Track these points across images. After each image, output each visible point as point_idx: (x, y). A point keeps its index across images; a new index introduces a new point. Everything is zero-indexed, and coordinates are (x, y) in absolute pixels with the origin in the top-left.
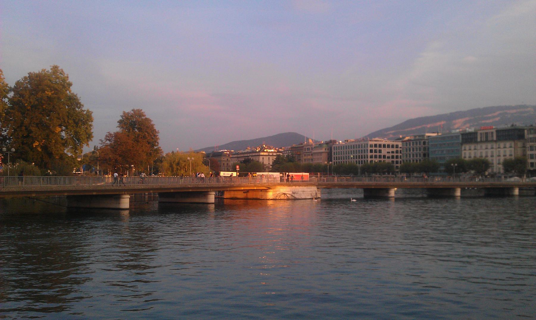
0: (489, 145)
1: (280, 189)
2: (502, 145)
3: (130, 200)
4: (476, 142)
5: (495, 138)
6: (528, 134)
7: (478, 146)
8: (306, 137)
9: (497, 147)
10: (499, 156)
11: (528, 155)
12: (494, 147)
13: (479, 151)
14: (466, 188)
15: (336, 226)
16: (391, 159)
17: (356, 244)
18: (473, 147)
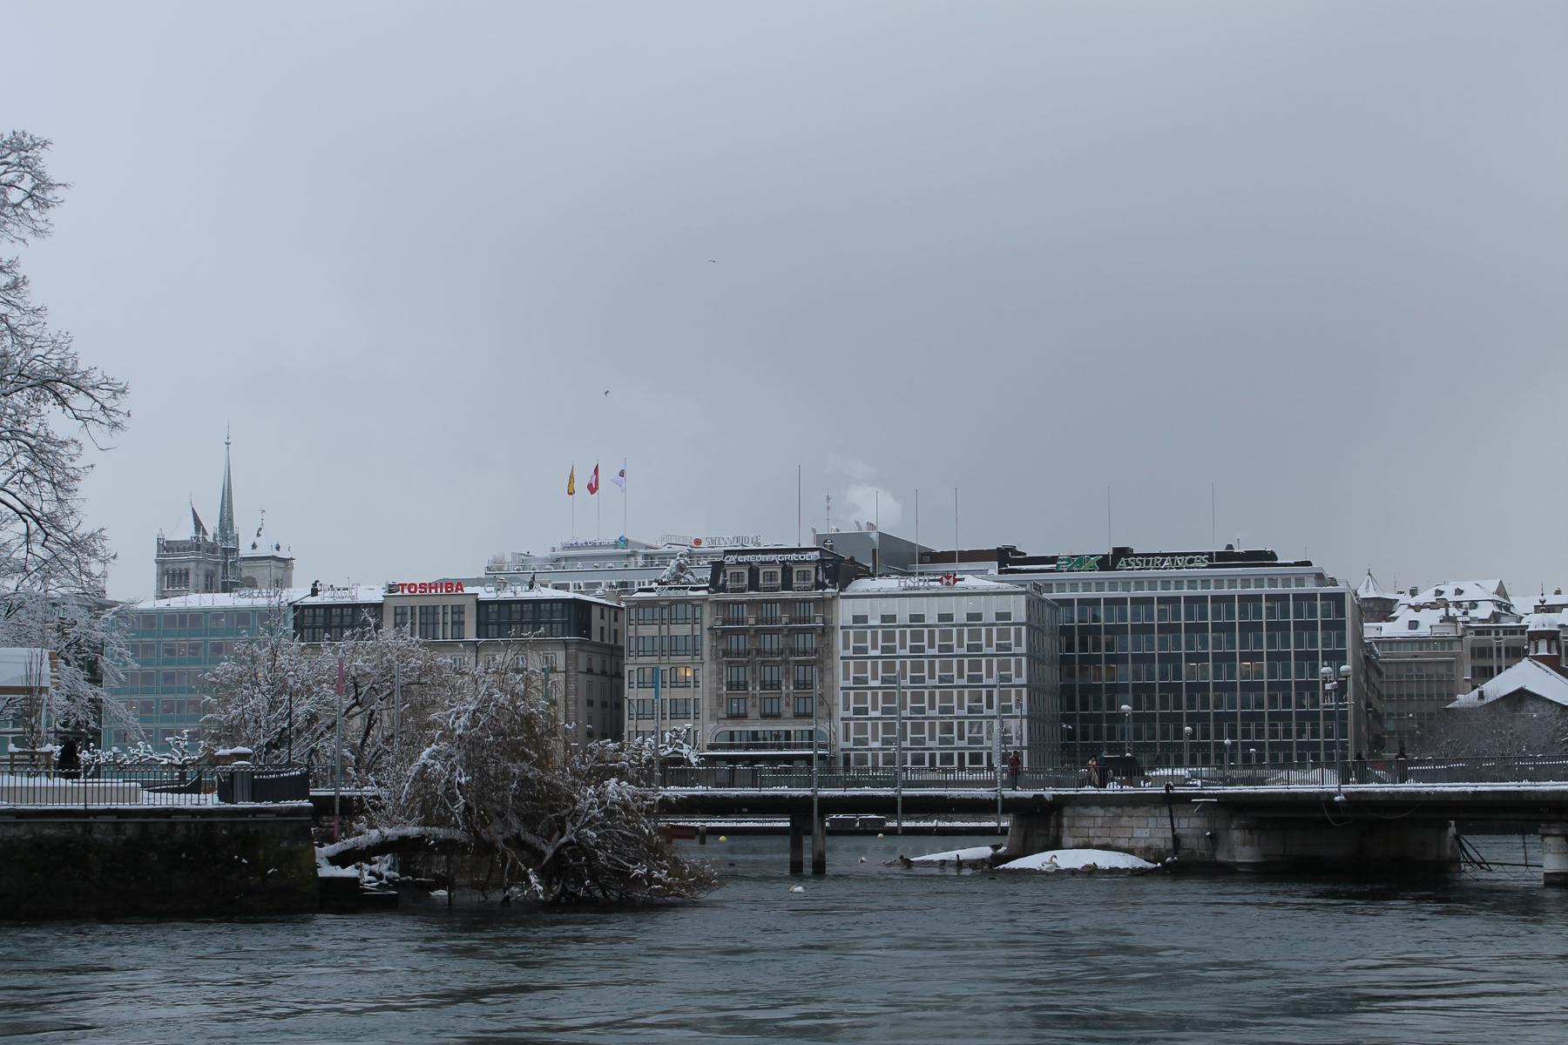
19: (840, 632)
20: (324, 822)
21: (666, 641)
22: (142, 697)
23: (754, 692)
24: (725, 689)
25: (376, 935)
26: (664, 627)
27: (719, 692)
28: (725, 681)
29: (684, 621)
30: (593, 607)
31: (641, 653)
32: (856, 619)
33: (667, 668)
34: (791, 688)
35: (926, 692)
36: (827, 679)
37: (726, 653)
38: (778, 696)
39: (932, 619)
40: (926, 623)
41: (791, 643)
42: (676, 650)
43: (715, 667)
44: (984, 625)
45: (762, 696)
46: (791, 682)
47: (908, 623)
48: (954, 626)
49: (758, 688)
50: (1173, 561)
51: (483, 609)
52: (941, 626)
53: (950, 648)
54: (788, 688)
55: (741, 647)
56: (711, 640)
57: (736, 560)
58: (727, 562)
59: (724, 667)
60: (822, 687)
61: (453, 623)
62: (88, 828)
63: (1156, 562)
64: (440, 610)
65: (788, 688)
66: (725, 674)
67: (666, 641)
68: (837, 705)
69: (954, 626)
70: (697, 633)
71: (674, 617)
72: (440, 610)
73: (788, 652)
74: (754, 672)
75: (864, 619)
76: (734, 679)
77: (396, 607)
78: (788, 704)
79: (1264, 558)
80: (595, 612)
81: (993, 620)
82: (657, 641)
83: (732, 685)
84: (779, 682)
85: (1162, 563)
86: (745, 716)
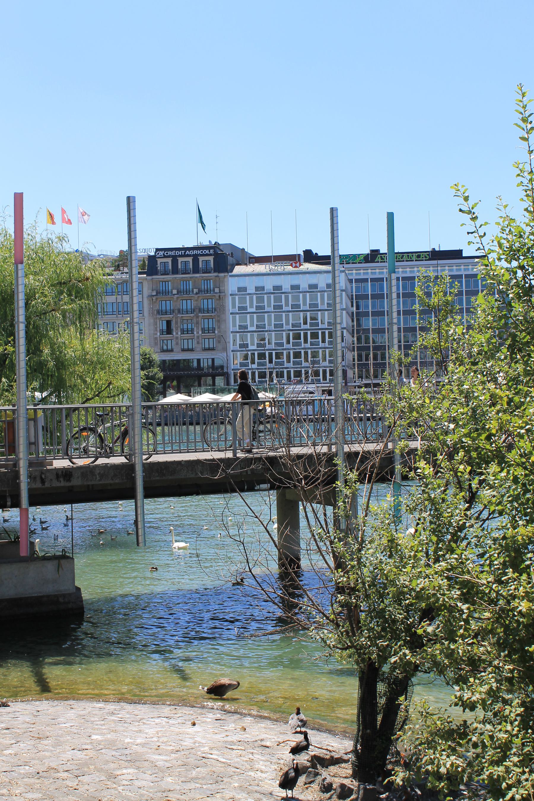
19: (230, 298)
20: (493, 677)
21: (120, 304)
22: (275, 454)
23: (177, 336)
24: (158, 334)
25: (302, 761)
27: (155, 336)
28: (158, 329)
29: (111, 294)
31: (106, 313)
32: (240, 289)
34: (200, 332)
35: (320, 332)
36: (223, 327)
38: (213, 337)
39: (251, 290)
40: (283, 291)
41: (199, 305)
42: (127, 311)
43: (152, 321)
44: (319, 292)
45: (203, 337)
46: (200, 328)
47: (272, 291)
48: (300, 292)
49: (179, 333)
50: (408, 256)
52: (293, 293)
54: (198, 333)
56: (150, 304)
57: (164, 254)
58: (158, 256)
59: (158, 320)
63: (398, 257)
65: (198, 333)
66: (158, 326)
67: (120, 304)
68: (229, 342)
69: (300, 292)
71: (125, 290)
73: (176, 311)
75: (245, 289)
76: (206, 326)
78: (198, 343)
79: (457, 254)
81: (254, 291)
82: (115, 305)
83: (183, 331)
84: (192, 330)
85: (402, 258)
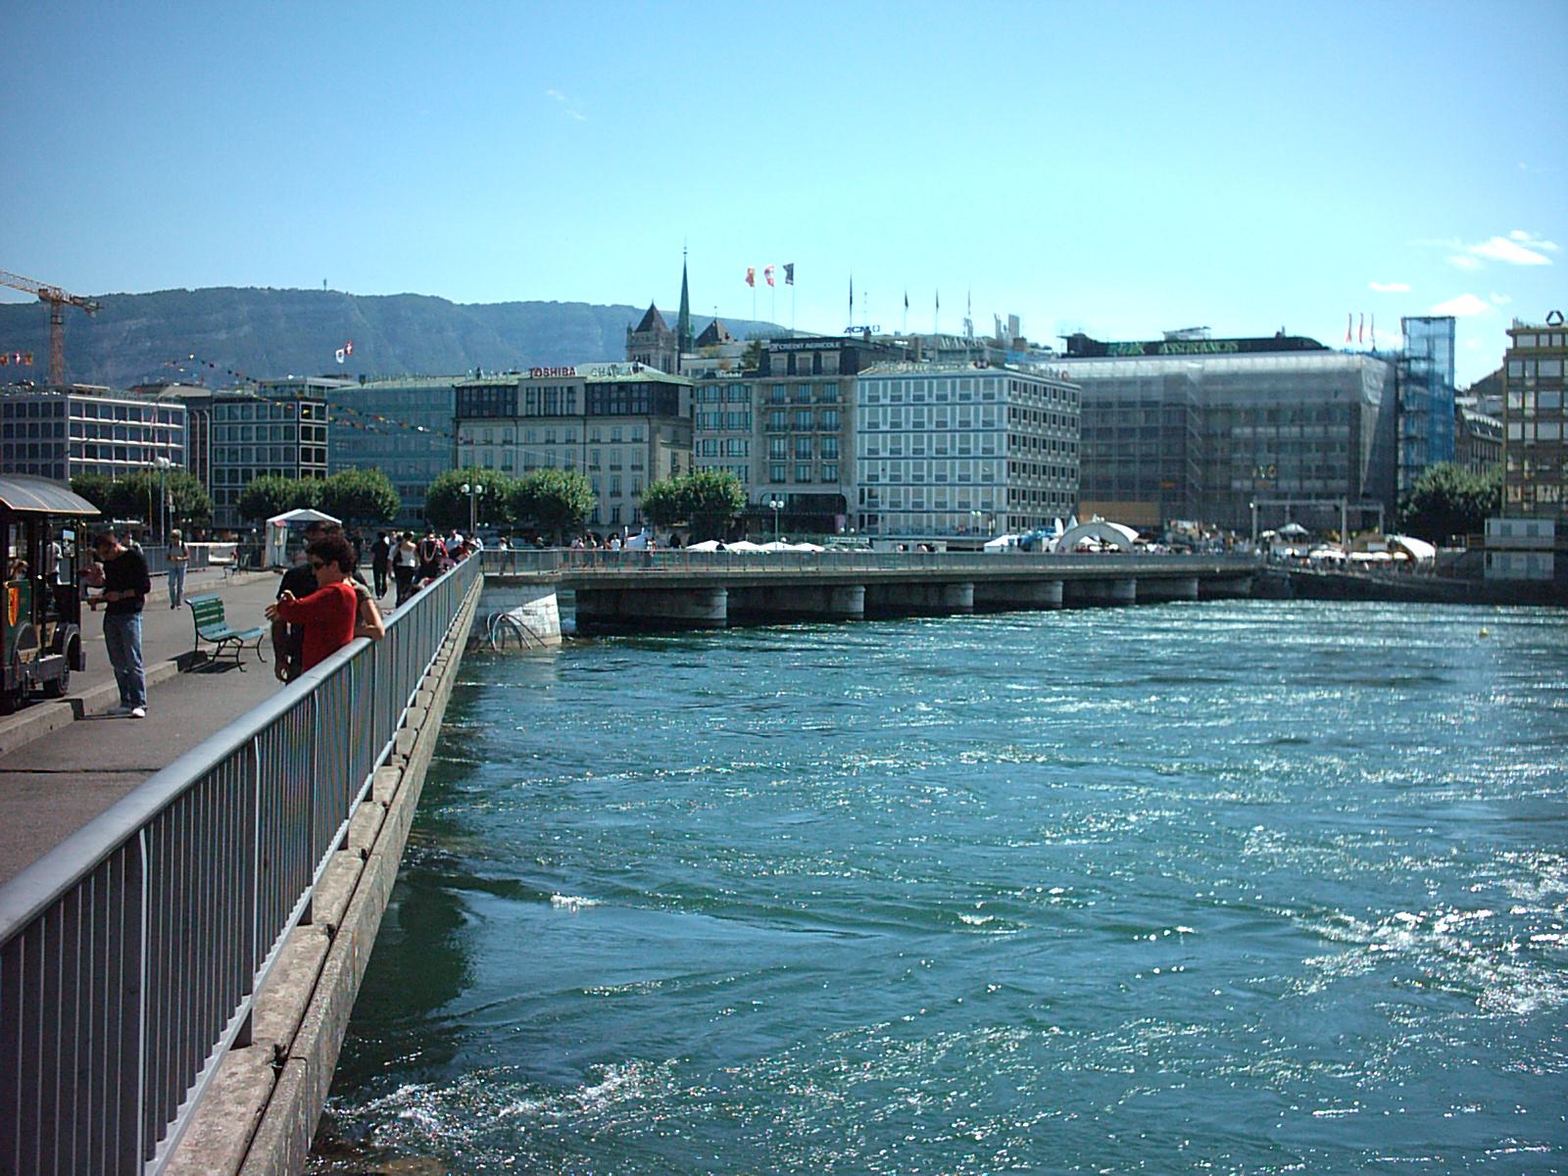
0: (561, 431)
1: (1507, 502)
2: (606, 430)
3: (1552, 441)
4: (514, 417)
5: (580, 409)
6: (808, 359)
7: (521, 431)
8: (25, 472)
9: (588, 440)
10: (616, 493)
11: (1050, 592)
12: (561, 437)
13: (522, 449)
14: (1039, 890)
15: (1228, 925)
16: (40, 464)
17: (642, 868)
18: (498, 431)
26: (723, 405)
30: (681, 388)
33: (700, 440)
37: (769, 428)
51: (590, 388)
53: (922, 424)
55: (782, 423)
60: (843, 457)
61: (568, 402)
62: (281, 647)
64: (559, 390)
70: (748, 410)
72: (559, 390)
74: (790, 443)
77: (1404, 320)
80: (683, 394)
86: (784, 481)
